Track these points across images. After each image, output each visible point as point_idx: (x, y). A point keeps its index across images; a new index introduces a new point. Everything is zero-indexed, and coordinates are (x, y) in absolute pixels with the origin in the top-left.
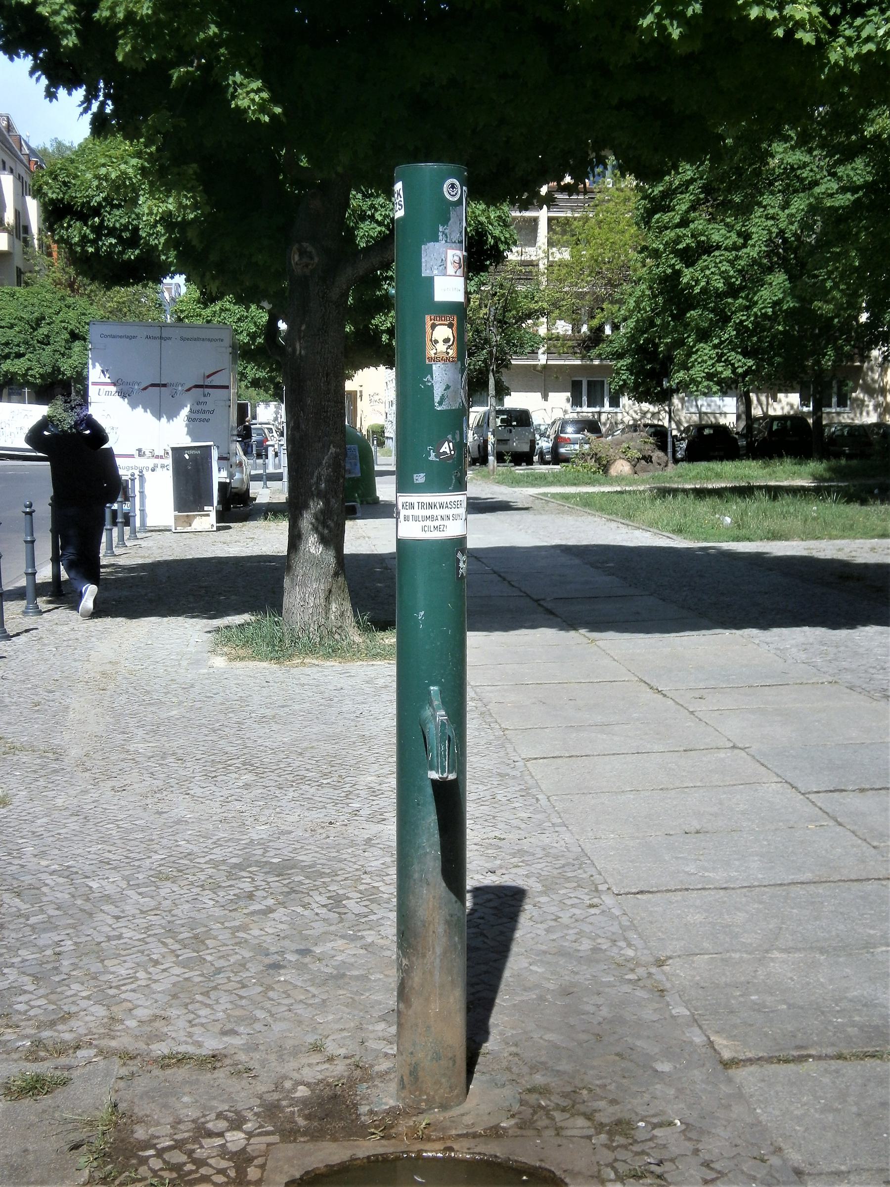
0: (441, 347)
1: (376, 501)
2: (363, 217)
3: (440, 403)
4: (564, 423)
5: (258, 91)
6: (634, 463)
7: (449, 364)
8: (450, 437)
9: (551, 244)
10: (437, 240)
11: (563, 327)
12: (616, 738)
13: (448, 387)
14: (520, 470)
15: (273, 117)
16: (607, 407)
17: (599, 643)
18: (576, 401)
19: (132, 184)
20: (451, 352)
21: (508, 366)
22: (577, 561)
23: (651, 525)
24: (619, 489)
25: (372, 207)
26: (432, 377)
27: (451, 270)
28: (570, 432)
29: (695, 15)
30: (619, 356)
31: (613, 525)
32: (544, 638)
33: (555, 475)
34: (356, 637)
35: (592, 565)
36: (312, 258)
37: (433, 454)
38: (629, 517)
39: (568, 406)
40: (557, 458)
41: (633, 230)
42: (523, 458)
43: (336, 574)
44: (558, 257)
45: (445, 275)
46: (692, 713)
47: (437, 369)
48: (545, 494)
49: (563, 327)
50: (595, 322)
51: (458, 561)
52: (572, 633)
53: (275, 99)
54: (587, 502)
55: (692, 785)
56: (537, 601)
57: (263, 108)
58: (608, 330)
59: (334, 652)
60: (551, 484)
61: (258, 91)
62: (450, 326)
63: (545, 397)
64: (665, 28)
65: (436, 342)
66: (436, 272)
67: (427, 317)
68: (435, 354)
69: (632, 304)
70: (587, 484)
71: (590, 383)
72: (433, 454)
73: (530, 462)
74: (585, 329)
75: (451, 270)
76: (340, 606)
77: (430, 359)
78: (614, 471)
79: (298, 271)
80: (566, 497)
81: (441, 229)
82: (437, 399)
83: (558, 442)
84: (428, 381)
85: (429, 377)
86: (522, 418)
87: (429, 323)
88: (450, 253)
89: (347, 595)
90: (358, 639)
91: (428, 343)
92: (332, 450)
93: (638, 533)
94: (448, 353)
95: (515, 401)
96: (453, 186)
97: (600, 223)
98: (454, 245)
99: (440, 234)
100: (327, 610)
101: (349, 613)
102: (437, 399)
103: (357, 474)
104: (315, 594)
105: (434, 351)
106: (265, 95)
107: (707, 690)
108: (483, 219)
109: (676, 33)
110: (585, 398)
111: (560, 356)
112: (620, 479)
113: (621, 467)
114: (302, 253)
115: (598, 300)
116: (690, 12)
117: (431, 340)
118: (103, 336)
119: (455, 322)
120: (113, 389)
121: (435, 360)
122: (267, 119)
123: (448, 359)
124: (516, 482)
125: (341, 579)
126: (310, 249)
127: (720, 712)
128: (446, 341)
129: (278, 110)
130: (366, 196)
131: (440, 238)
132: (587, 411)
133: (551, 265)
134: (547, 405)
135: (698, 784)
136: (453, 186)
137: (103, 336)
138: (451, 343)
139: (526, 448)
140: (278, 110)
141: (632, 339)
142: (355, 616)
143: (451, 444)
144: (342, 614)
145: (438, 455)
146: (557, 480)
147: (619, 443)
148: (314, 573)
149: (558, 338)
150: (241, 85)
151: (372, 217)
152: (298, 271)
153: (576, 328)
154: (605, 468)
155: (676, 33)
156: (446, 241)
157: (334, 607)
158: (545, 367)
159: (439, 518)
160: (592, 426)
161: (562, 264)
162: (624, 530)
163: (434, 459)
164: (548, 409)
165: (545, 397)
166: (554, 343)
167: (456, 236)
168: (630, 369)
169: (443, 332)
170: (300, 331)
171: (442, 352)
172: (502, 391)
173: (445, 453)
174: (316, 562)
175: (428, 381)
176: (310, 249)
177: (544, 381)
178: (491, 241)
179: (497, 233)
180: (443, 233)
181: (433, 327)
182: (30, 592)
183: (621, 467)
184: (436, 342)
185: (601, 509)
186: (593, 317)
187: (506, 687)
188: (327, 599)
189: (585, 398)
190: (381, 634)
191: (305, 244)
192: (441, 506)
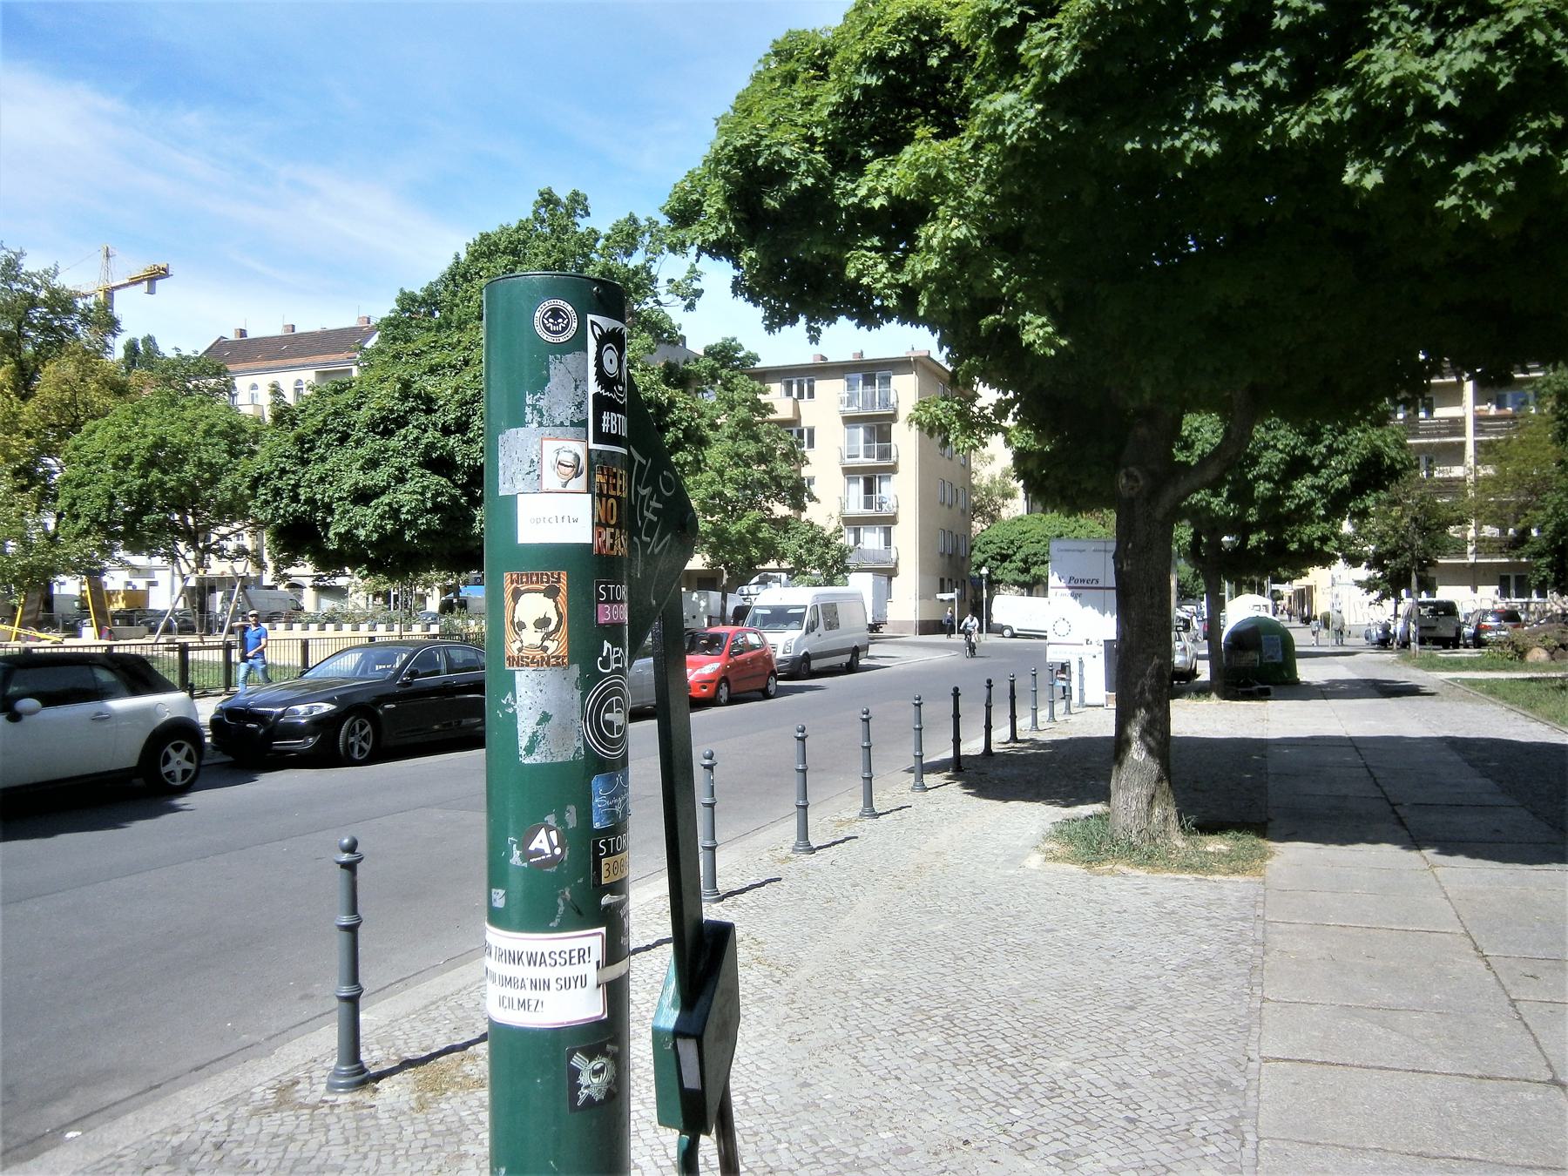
0: (532, 637)
1: (1297, 682)
2: (1266, 447)
3: (530, 750)
4: (1485, 613)
5: (1043, 326)
6: (1552, 652)
7: (548, 672)
8: (551, 819)
9: (1477, 462)
10: (522, 424)
11: (1490, 531)
12: (1395, 1037)
13: (545, 718)
14: (1443, 654)
15: (1059, 349)
16: (1535, 598)
17: (1438, 871)
18: (1505, 593)
19: (941, 425)
20: (552, 646)
21: (1433, 564)
22: (1455, 757)
23: (1549, 718)
24: (1528, 675)
25: (1274, 438)
26: (514, 696)
27: (552, 479)
28: (1490, 621)
29: (1506, 193)
30: (1539, 555)
31: (1513, 715)
32: (1387, 855)
33: (1470, 660)
34: (1179, 841)
35: (1471, 763)
36: (1137, 481)
37: (517, 853)
38: (1530, 707)
39: (1497, 598)
40: (1478, 642)
41: (1554, 447)
42: (1453, 642)
43: (1160, 780)
44: (1482, 473)
45: (539, 491)
46: (1513, 1002)
47: (524, 680)
48: (1455, 680)
49: (1490, 531)
50: (1520, 526)
51: (576, 1073)
52: (1414, 854)
53: (1061, 332)
54: (1492, 690)
55: (1466, 1154)
56: (1393, 805)
57: (1048, 341)
58: (1534, 532)
59: (1148, 860)
60: (1466, 669)
61: (1043, 326)
62: (551, 593)
63: (1475, 590)
64: (1471, 208)
65: (522, 626)
66: (520, 486)
67: (507, 576)
68: (520, 650)
69: (1550, 510)
70: (1500, 669)
71: (1517, 578)
72: (517, 853)
73: (1456, 646)
74: (1511, 531)
75: (552, 479)
76: (1165, 811)
77: (512, 660)
78: (1529, 658)
79: (1126, 494)
80: (1473, 683)
81: (529, 400)
82: (523, 742)
83: (1479, 630)
84: (509, 705)
85: (509, 696)
86: (1449, 609)
87: (509, 589)
88: (550, 447)
89: (1171, 800)
90: (1180, 843)
91: (508, 626)
92: (1156, 661)
93: (1535, 726)
94: (545, 649)
95: (1444, 593)
96: (555, 313)
97: (1522, 443)
98: (559, 431)
99: (528, 410)
100: (1149, 814)
101: (1173, 818)
102: (523, 742)
103: (1279, 659)
104: (1137, 797)
105: (518, 645)
106: (1050, 329)
107: (1546, 963)
108: (1379, 443)
109: (1485, 213)
110: (1513, 591)
111: (1487, 555)
112: (1537, 666)
113: (1538, 655)
114: (1129, 476)
115: (1522, 508)
116: (1500, 189)
117: (512, 622)
118: (1060, 550)
119: (563, 586)
120: (1068, 592)
121: (518, 661)
122: (1053, 352)
123: (546, 662)
124: (1432, 666)
125: (1165, 784)
126: (1136, 473)
127: (1551, 1007)
128: (542, 623)
129: (1063, 342)
130: (1268, 429)
131: (529, 417)
132: (1515, 602)
133: (1477, 479)
134: (1477, 596)
135: (1476, 1156)
136: (555, 313)
137: (1060, 550)
138: (552, 627)
139: (1453, 634)
140: (1063, 342)
141: (1553, 540)
142: (1180, 820)
143: (553, 835)
144: (1166, 819)
145: (527, 855)
146: (1471, 665)
147: (1535, 633)
148: (1137, 778)
149: (1484, 540)
150: (1029, 323)
151: (1275, 446)
152: (1126, 494)
153: (1504, 532)
154: (1521, 653)
155: (1485, 213)
156: (540, 424)
157: (1157, 811)
158: (1474, 565)
159: (528, 983)
160: (1511, 616)
161: (1487, 478)
162: (1521, 721)
163: (520, 863)
164: (1474, 601)
165: (1475, 590)
166: (1483, 545)
167: (565, 412)
168: (1550, 566)
169: (534, 606)
170: (1126, 549)
171: (531, 647)
172: (1428, 586)
173: (539, 852)
174: (1139, 768)
175: (509, 705)
176: (1136, 473)
177: (1473, 576)
178: (1388, 461)
179: (1393, 454)
180: (534, 407)
181: (517, 595)
182: (918, 769)
183: (1538, 655)
184: (522, 626)
185: (1505, 698)
186: (1517, 522)
187: (1302, 928)
188: (1151, 803)
189: (1513, 591)
190: (1207, 838)
191: (1131, 469)
192: (532, 960)
